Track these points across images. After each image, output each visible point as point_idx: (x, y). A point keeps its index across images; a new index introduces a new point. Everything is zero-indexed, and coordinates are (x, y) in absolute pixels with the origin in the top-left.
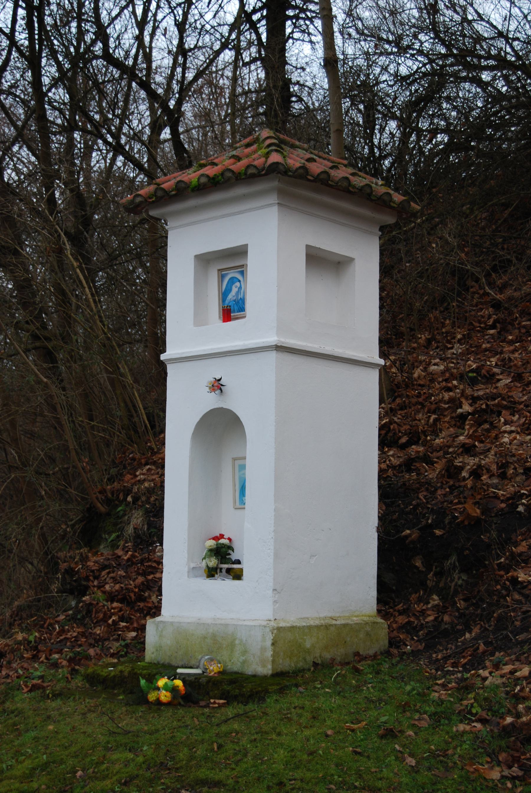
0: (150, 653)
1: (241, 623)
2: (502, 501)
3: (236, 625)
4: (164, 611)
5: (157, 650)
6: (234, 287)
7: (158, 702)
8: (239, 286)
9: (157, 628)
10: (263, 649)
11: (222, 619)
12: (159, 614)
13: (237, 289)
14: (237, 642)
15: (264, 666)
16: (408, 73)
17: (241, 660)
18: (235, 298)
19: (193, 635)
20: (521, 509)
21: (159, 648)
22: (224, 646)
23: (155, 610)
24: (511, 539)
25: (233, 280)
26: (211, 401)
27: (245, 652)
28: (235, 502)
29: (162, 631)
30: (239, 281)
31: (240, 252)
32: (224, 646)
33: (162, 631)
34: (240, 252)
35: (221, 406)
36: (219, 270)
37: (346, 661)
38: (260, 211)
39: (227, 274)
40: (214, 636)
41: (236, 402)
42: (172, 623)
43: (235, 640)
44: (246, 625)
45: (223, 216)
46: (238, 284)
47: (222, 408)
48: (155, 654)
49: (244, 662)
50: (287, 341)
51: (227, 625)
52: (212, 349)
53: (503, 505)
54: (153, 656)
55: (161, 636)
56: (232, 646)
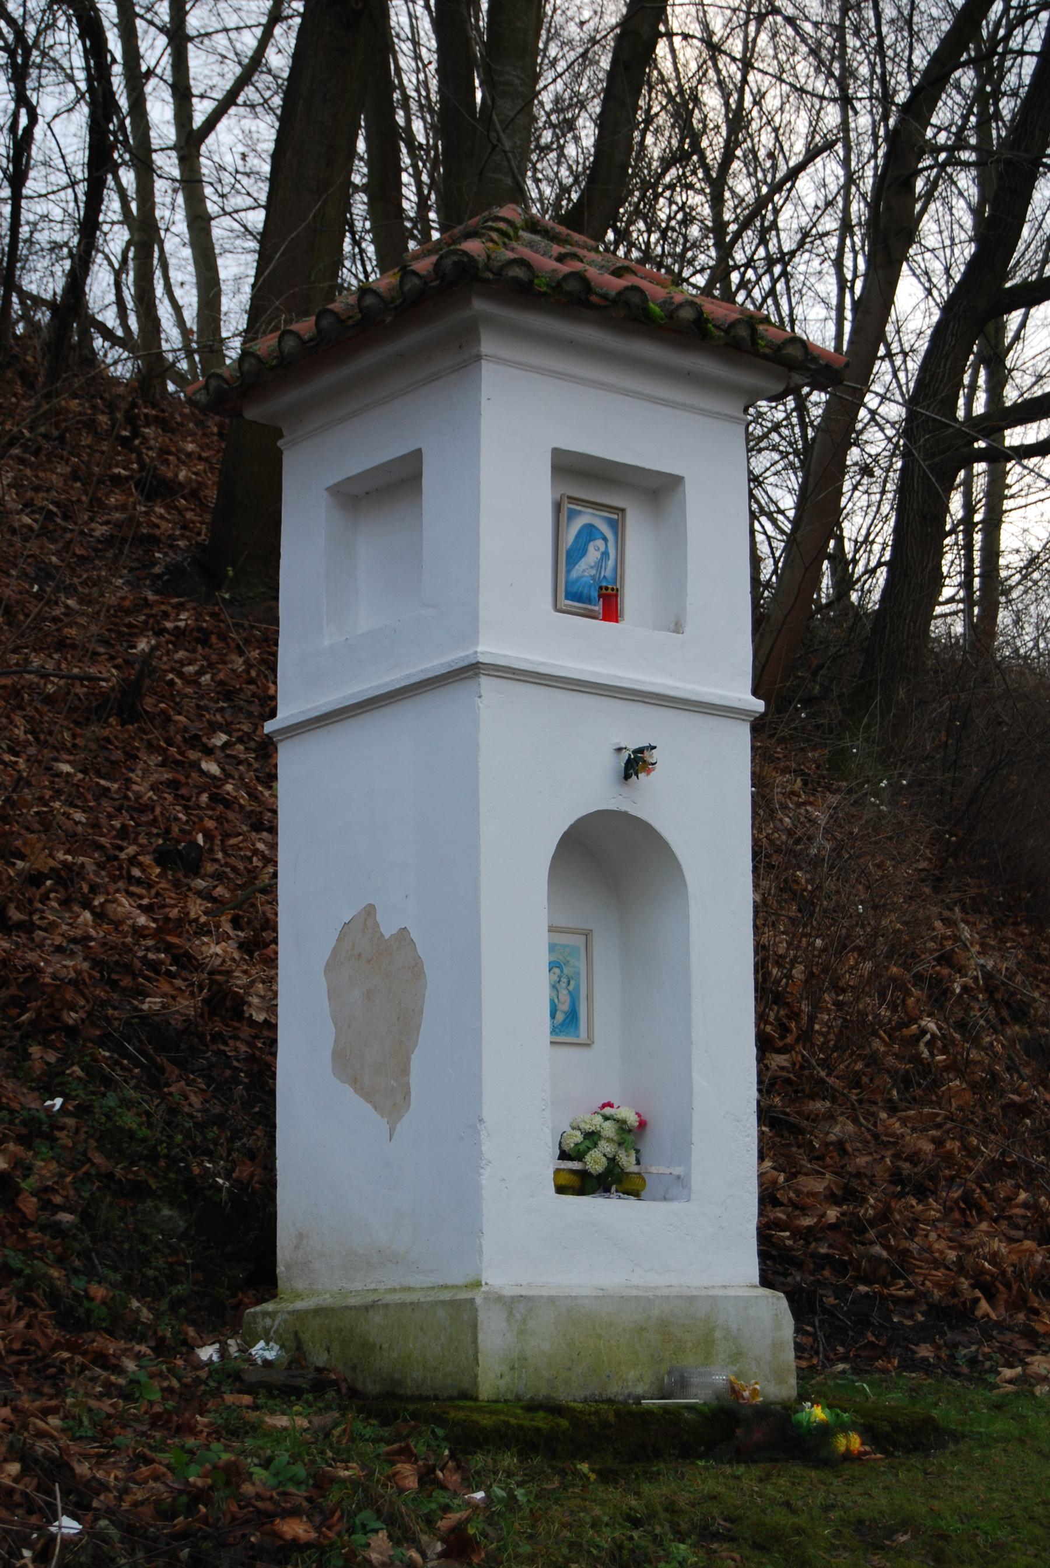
0: (492, 1376)
1: (721, 1292)
3: (714, 1298)
5: (512, 1368)
6: (591, 547)
8: (603, 549)
9: (510, 1314)
10: (777, 1346)
13: (598, 555)
14: (718, 1334)
15: (781, 1381)
16: (25, 192)
18: (593, 572)
21: (518, 1363)
22: (689, 1345)
25: (589, 533)
26: (596, 791)
27: (737, 1356)
29: (524, 1320)
30: (605, 539)
33: (524, 1320)
35: (623, 809)
39: (579, 512)
40: (664, 1325)
41: (653, 801)
42: (552, 1300)
43: (712, 1330)
44: (735, 1297)
45: (627, 393)
46: (600, 543)
48: (507, 1378)
50: (620, 673)
51: (692, 1299)
52: (542, 664)
54: (502, 1383)
55: (522, 1333)
56: (707, 1344)
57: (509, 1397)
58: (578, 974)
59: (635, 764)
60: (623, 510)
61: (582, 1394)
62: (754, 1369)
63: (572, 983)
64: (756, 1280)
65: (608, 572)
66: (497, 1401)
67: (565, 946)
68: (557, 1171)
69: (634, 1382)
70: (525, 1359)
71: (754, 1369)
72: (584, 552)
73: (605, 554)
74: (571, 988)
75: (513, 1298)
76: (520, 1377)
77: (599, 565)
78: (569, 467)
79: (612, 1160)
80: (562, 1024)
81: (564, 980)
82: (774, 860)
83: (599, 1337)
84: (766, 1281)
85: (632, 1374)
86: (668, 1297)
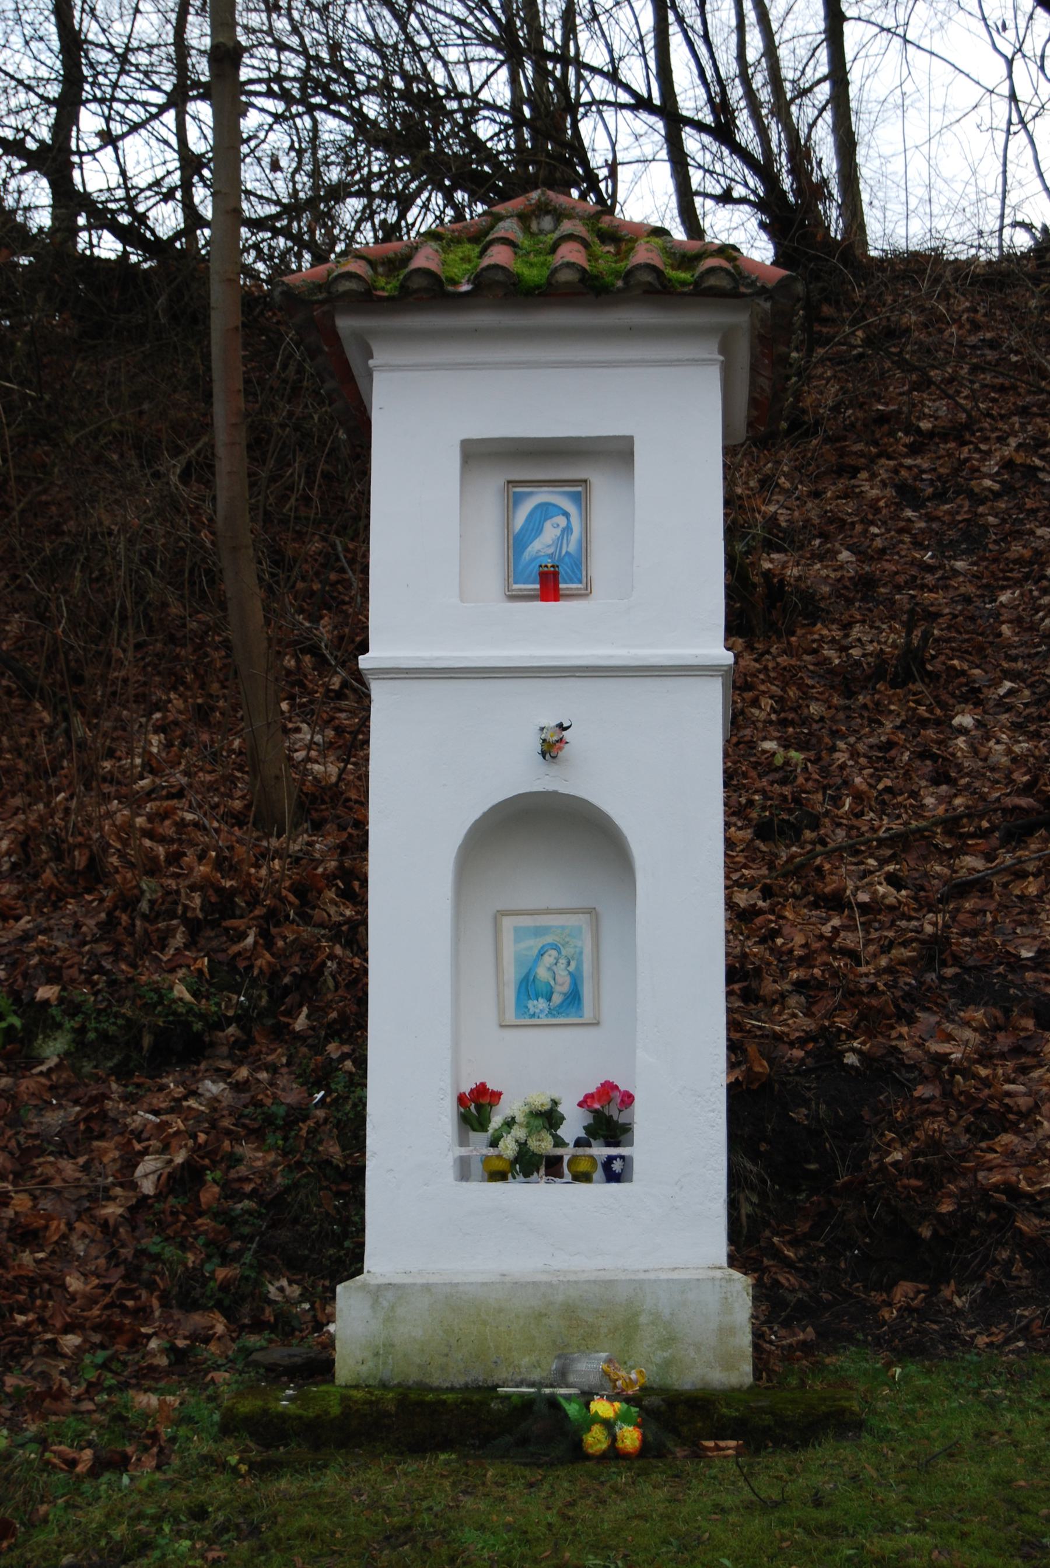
2: (792, 1044)
4: (368, 1263)
6: (548, 525)
7: (614, 1454)
10: (726, 1331)
11: (575, 1273)
12: (360, 1271)
13: (558, 532)
14: (643, 1319)
17: (658, 1360)
18: (551, 550)
19: (500, 1310)
20: (851, 1059)
21: (382, 1350)
22: (604, 1330)
23: (350, 1261)
24: (862, 1117)
25: (545, 511)
27: (670, 1340)
28: (501, 1010)
29: (392, 1308)
30: (566, 514)
31: (619, 453)
32: (604, 1330)
33: (392, 1308)
34: (619, 453)
36: (509, 482)
37: (490, 1384)
38: (620, 370)
40: (570, 1312)
42: (427, 1288)
43: (636, 1314)
46: (562, 521)
47: (555, 793)
48: (370, 1364)
49: (668, 1363)
51: (610, 1283)
52: (438, 658)
53: (798, 1053)
54: (364, 1369)
55: (388, 1320)
57: (371, 1382)
58: (581, 953)
59: (551, 748)
60: (585, 481)
61: (460, 1381)
62: (692, 1354)
63: (573, 964)
64: (723, 1261)
65: (572, 547)
66: (356, 1387)
67: (563, 928)
68: (631, 1144)
69: (453, 1373)
70: (392, 1346)
71: (692, 1354)
72: (539, 531)
73: (568, 530)
74: (572, 968)
75: (379, 1286)
76: (385, 1363)
77: (559, 541)
78: (477, 454)
79: (522, 1145)
80: (561, 1006)
81: (563, 961)
82: (770, 825)
83: (485, 1323)
84: (733, 1261)
85: (526, 1361)
86: (576, 1282)
